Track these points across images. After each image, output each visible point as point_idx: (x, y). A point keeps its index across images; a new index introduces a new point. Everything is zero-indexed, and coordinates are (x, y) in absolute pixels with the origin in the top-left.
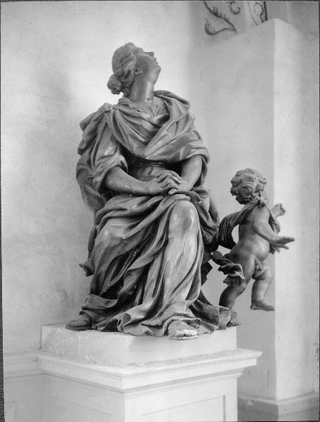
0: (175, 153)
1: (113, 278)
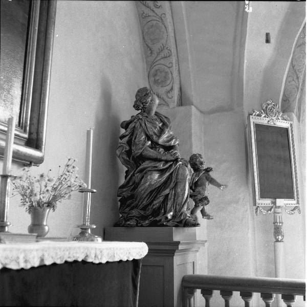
1: (147, 200)
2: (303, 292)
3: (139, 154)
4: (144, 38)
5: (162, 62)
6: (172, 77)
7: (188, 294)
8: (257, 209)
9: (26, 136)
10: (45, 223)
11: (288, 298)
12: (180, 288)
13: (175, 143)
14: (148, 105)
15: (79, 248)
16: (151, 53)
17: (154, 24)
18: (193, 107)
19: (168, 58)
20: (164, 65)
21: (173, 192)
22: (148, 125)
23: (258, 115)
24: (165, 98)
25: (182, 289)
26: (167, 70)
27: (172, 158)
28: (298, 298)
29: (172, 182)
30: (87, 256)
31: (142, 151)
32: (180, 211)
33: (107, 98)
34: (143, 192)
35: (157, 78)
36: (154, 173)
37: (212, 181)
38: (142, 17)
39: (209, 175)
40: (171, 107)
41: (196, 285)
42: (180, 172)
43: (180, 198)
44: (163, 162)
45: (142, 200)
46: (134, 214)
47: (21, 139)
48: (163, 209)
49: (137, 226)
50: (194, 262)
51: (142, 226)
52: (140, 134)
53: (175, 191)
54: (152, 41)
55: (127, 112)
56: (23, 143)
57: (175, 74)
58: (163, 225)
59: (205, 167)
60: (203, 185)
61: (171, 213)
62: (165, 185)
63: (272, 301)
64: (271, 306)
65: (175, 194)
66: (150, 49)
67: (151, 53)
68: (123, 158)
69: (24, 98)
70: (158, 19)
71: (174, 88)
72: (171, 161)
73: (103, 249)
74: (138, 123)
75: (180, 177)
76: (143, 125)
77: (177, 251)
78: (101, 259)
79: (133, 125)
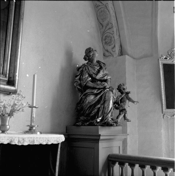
0: (161, 67)
1: (88, 111)
2: (173, 167)
3: (84, 86)
4: (98, 19)
5: (108, 31)
6: (114, 39)
7: (112, 165)
8: (164, 115)
9: (7, 79)
10: (7, 124)
11: (165, 169)
12: (106, 162)
13: (107, 78)
14: (91, 57)
15: (5, 137)
16: (103, 27)
17: (103, 10)
18: (127, 56)
19: (111, 29)
20: (109, 33)
21: (103, 106)
22: (90, 69)
23: (165, 58)
24: (111, 52)
25: (108, 162)
26: (111, 35)
27: (102, 87)
28: (171, 170)
29: (102, 100)
30: (11, 141)
31: (85, 83)
32: (106, 116)
33: (69, 55)
34: (85, 107)
35: (106, 41)
36: (91, 96)
37: (130, 99)
38: (96, 6)
39: (128, 96)
40: (115, 57)
41: (116, 160)
42: (107, 95)
43: (106, 110)
44: (97, 90)
45: (85, 111)
46: (81, 119)
47: (4, 81)
48: (97, 116)
49: (82, 125)
50: (119, 147)
51: (85, 125)
52: (85, 74)
53: (104, 106)
54: (102, 19)
55: (81, 61)
56: (5, 83)
57: (116, 37)
58: (95, 125)
59: (127, 90)
60: (124, 101)
61: (100, 118)
62: (98, 102)
63: (169, 173)
64: (168, 175)
65: (104, 107)
66: (102, 25)
67: (103, 27)
68: (77, 88)
69: (5, 60)
70: (104, 7)
71: (115, 46)
72: (102, 89)
73: (25, 138)
74: (84, 68)
75: (107, 98)
76: (87, 69)
77: (100, 140)
78: (23, 143)
79: (81, 69)
